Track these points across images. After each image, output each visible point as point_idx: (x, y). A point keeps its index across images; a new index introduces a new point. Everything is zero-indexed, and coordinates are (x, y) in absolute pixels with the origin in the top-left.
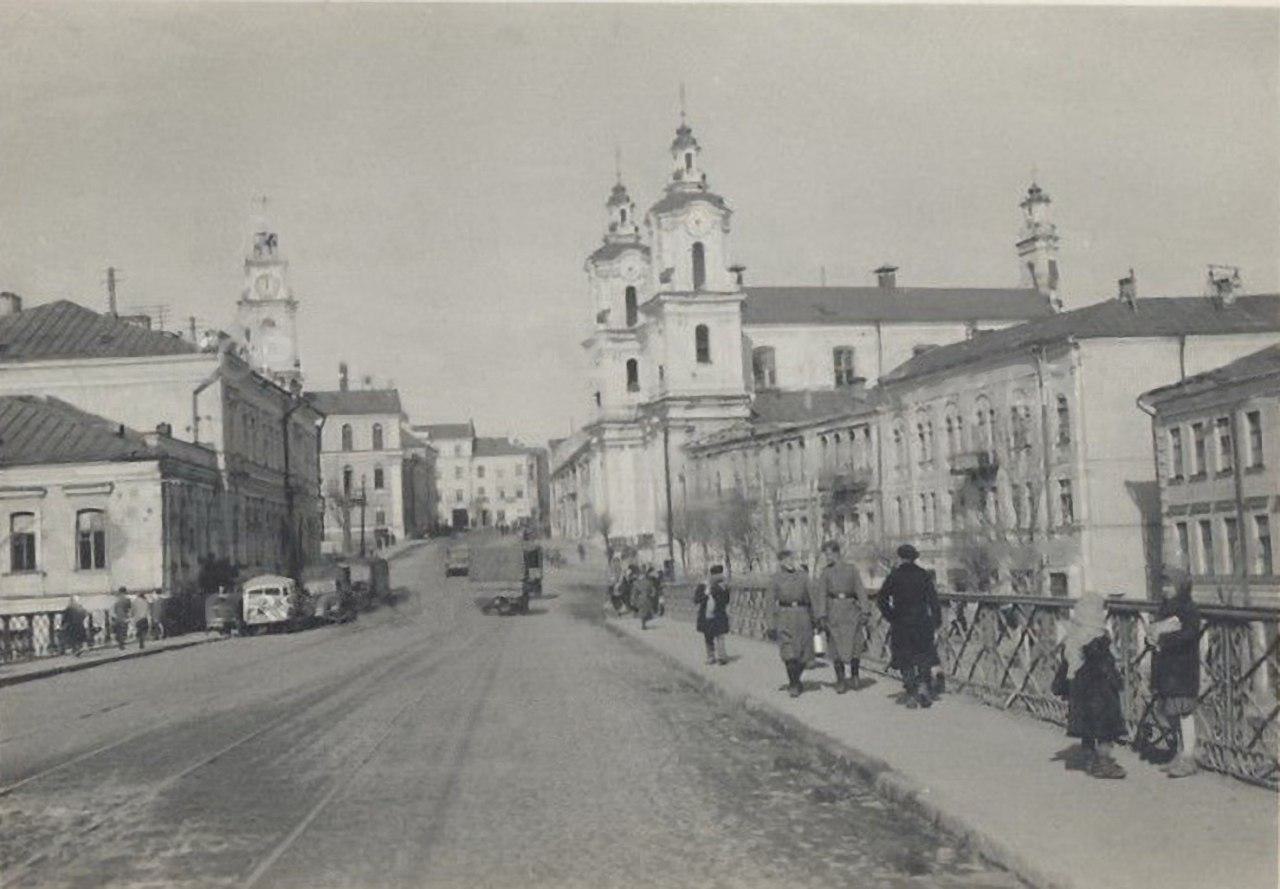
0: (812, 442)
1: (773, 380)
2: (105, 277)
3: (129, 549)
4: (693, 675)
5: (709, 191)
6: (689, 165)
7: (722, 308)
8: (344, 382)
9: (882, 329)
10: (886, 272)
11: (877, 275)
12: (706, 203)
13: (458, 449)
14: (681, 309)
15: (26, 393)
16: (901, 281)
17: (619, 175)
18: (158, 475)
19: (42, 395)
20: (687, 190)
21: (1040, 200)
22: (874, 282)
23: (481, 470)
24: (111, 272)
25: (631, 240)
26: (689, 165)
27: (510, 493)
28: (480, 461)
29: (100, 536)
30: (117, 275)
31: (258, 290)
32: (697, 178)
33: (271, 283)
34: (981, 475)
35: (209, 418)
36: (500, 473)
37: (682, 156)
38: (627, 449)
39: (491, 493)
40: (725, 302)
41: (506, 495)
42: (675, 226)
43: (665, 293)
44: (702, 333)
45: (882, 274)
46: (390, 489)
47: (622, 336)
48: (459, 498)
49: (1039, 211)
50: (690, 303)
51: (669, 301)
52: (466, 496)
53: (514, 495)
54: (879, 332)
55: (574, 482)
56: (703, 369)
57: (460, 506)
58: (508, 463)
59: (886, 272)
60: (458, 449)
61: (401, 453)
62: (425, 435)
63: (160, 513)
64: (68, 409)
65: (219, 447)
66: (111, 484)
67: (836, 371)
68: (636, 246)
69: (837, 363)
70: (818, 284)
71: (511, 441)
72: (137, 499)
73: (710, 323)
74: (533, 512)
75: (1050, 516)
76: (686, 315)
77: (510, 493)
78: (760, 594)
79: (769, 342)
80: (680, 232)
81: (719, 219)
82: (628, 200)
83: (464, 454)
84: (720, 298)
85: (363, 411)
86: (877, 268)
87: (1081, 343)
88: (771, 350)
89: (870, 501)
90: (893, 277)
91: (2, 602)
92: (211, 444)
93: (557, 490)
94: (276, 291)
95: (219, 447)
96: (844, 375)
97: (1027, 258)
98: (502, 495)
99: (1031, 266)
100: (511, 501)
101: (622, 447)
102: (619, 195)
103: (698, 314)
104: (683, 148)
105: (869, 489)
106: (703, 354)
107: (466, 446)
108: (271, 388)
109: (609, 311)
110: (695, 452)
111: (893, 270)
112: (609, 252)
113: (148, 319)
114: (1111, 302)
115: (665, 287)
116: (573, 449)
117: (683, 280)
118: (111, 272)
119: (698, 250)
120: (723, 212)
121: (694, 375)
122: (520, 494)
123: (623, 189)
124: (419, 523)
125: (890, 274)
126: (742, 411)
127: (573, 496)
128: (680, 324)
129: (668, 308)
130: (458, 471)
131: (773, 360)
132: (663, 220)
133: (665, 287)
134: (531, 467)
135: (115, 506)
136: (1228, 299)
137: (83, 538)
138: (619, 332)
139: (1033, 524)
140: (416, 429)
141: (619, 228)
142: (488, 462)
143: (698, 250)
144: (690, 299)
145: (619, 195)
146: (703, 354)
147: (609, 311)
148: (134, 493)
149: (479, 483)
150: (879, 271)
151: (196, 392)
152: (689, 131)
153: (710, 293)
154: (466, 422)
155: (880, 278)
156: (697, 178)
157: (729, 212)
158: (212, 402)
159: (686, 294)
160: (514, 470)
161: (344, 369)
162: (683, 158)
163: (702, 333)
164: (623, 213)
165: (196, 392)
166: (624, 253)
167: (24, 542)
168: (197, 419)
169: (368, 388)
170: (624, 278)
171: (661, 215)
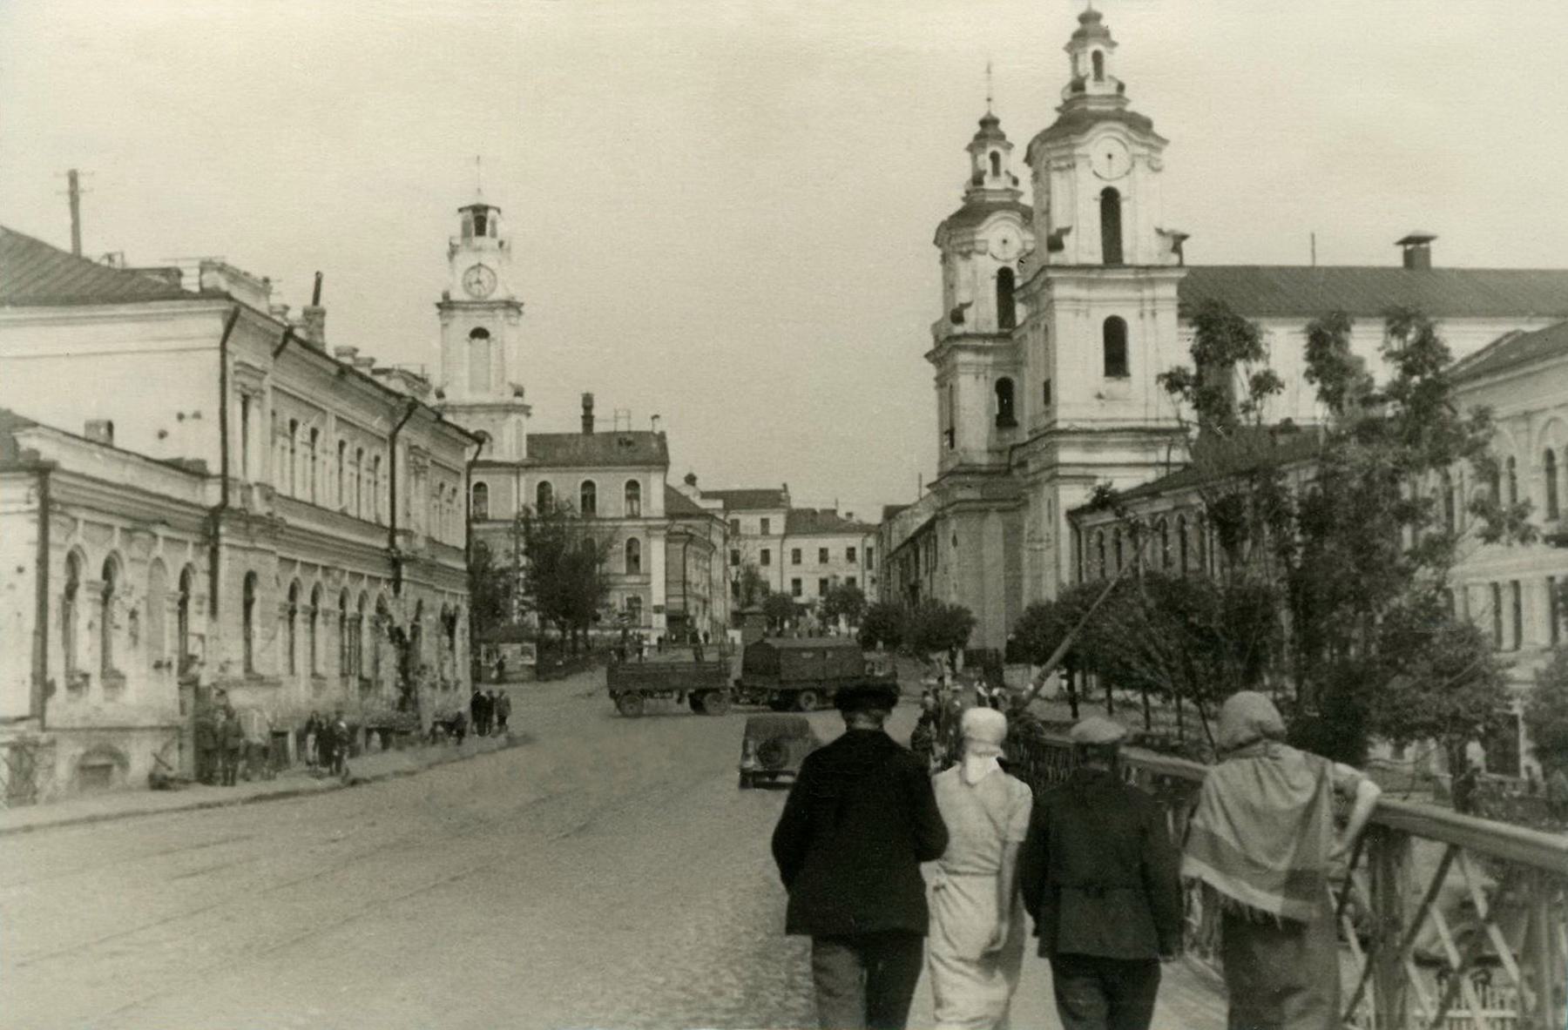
2: (65, 184)
5: (1129, 108)
8: (588, 420)
10: (1415, 246)
11: (1401, 249)
13: (765, 522)
14: (1082, 293)
16: (1440, 257)
20: (1092, 108)
22: (1395, 259)
24: (73, 178)
25: (1006, 199)
28: (792, 543)
30: (83, 182)
32: (1111, 89)
36: (824, 555)
44: (1115, 333)
45: (1409, 247)
46: (648, 575)
51: (1063, 281)
56: (1116, 386)
58: (837, 545)
59: (1415, 246)
60: (765, 522)
61: (665, 522)
62: (719, 504)
68: (1013, 206)
70: (1305, 261)
71: (841, 514)
73: (1129, 315)
80: (1083, 173)
85: (607, 463)
90: (1427, 251)
91: (5, 728)
92: (202, 463)
102: (989, 128)
103: (1115, 300)
107: (778, 522)
108: (355, 381)
111: (1427, 239)
112: (972, 213)
113: (180, 274)
116: (923, 520)
117: (1085, 245)
118: (73, 178)
123: (995, 122)
124: (706, 620)
125: (1423, 246)
128: (1077, 312)
129: (1060, 291)
140: (705, 495)
142: (810, 546)
144: (1094, 275)
145: (989, 128)
150: (1405, 242)
152: (1098, 17)
154: (777, 486)
156: (1111, 89)
160: (844, 553)
163: (1115, 333)
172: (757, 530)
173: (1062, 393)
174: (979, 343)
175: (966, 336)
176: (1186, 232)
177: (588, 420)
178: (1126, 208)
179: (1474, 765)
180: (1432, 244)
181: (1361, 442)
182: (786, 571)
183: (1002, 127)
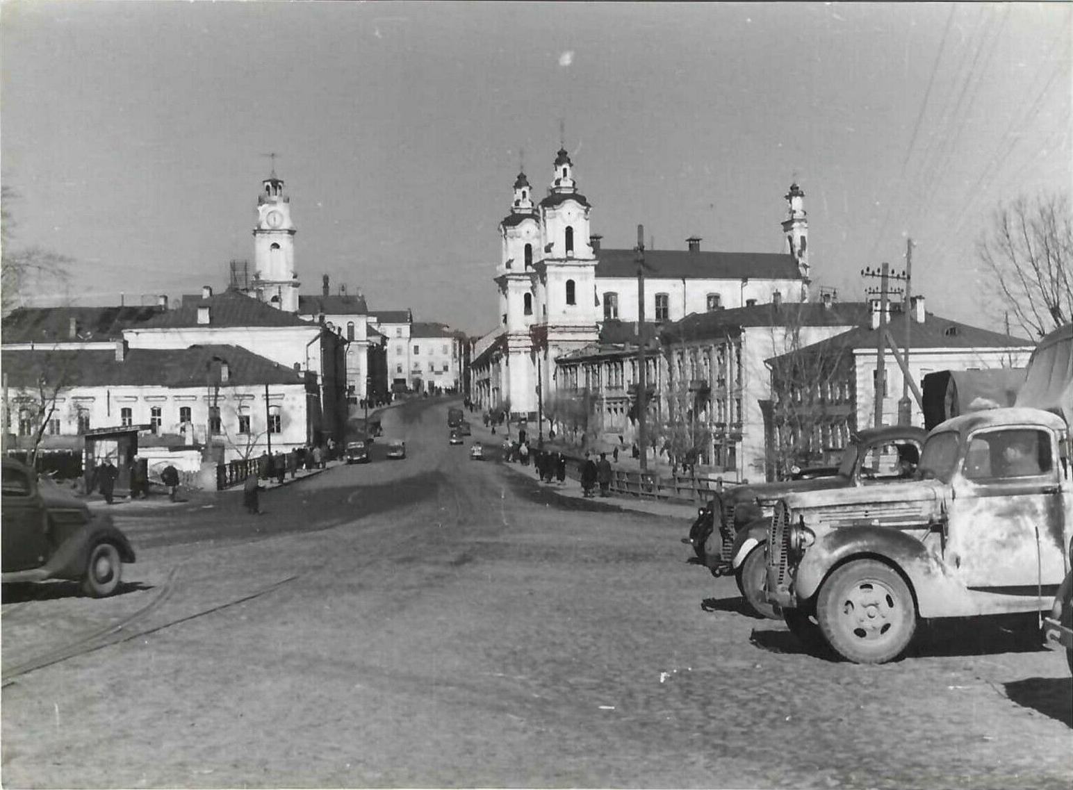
0: (627, 365)
1: (616, 314)
3: (291, 424)
4: (607, 547)
6: (565, 175)
7: (583, 269)
8: (326, 286)
9: (686, 281)
10: (694, 242)
12: (575, 202)
13: (399, 331)
15: (225, 343)
16: (704, 247)
17: (522, 167)
18: (305, 391)
19: (234, 345)
21: (796, 195)
23: (416, 348)
25: (530, 212)
26: (565, 175)
27: (439, 368)
28: (416, 342)
29: (278, 418)
31: (268, 223)
33: (277, 216)
34: (703, 394)
35: (314, 358)
37: (560, 169)
38: (523, 354)
39: (424, 367)
40: (584, 266)
41: (435, 369)
42: (554, 217)
43: (547, 260)
44: (570, 286)
47: (521, 277)
48: (399, 370)
49: (797, 203)
50: (562, 266)
51: (549, 265)
52: (404, 369)
53: (442, 369)
54: (684, 283)
55: (490, 373)
56: (569, 308)
57: (400, 376)
59: (694, 242)
60: (399, 331)
63: (305, 407)
64: (247, 352)
65: (319, 373)
66: (284, 395)
67: (657, 309)
69: (658, 303)
72: (294, 401)
74: (456, 383)
75: (732, 418)
76: (561, 273)
77: (439, 368)
78: (803, 461)
79: (613, 289)
80: (558, 219)
81: (583, 212)
82: (528, 185)
83: (403, 335)
84: (582, 263)
86: (688, 238)
87: (746, 329)
88: (615, 294)
89: (654, 401)
92: (315, 372)
93: (475, 376)
94: (281, 223)
95: (319, 373)
96: (662, 311)
97: (789, 233)
98: (432, 369)
99: (790, 239)
100: (438, 373)
101: (520, 352)
103: (569, 272)
104: (561, 165)
105: (654, 394)
106: (571, 299)
107: (406, 329)
109: (513, 260)
110: (562, 363)
111: (698, 240)
114: (769, 304)
115: (548, 255)
117: (559, 250)
119: (569, 231)
120: (585, 208)
121: (564, 312)
122: (446, 368)
126: (595, 337)
127: (487, 381)
130: (399, 351)
131: (616, 301)
132: (547, 212)
133: (548, 255)
134: (455, 345)
135: (285, 404)
136: (828, 305)
137: (270, 419)
138: (520, 275)
139: (739, 420)
141: (520, 203)
142: (425, 344)
143: (569, 231)
146: (571, 299)
147: (513, 260)
148: (294, 399)
149: (414, 358)
150: (690, 240)
151: (308, 345)
152: (566, 153)
153: (576, 259)
154: (405, 310)
155: (690, 245)
157: (589, 206)
158: (316, 350)
159: (560, 260)
160: (441, 349)
161: (326, 279)
162: (562, 172)
163: (570, 286)
164: (524, 193)
165: (308, 345)
166: (524, 221)
167: (245, 420)
168: (308, 359)
169: (342, 294)
170: (523, 239)
171: (546, 208)
172: (395, 334)
173: (550, 311)
174: (517, 277)
175: (512, 274)
176: (601, 235)
177: (326, 286)
178: (575, 235)
179: (401, 444)
180: (700, 242)
181: (522, 463)
182: (411, 359)
183: (528, 179)
